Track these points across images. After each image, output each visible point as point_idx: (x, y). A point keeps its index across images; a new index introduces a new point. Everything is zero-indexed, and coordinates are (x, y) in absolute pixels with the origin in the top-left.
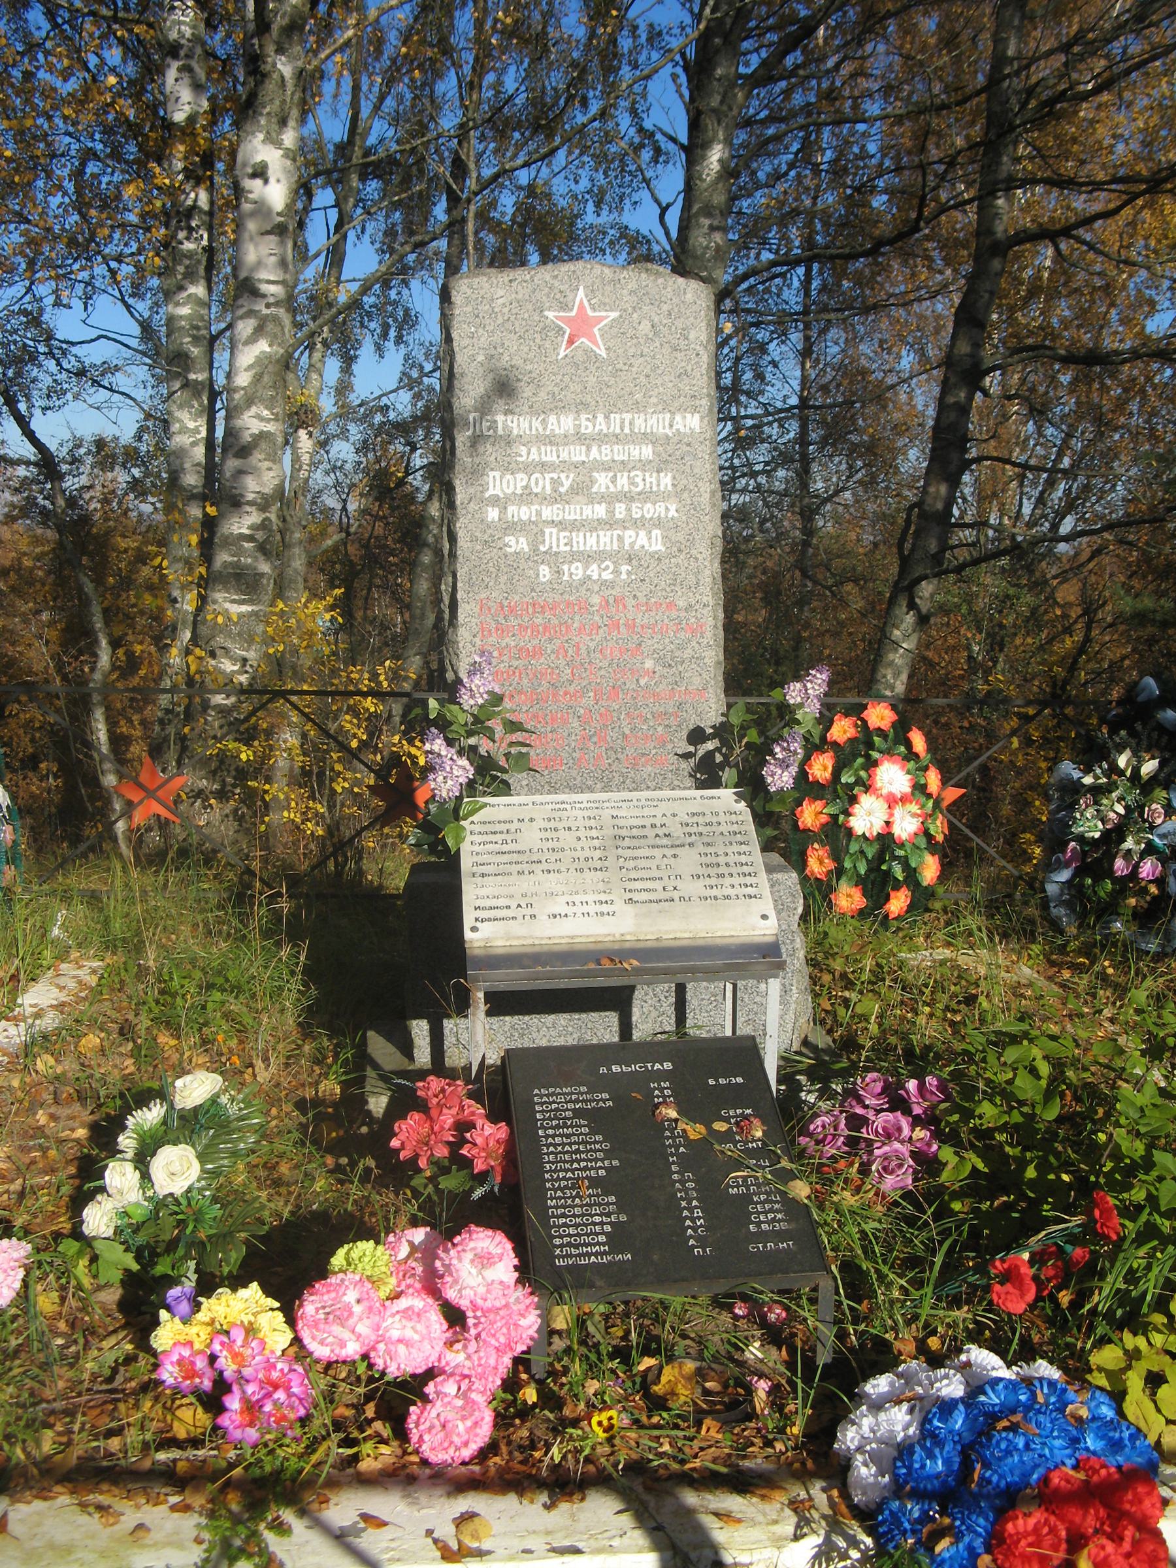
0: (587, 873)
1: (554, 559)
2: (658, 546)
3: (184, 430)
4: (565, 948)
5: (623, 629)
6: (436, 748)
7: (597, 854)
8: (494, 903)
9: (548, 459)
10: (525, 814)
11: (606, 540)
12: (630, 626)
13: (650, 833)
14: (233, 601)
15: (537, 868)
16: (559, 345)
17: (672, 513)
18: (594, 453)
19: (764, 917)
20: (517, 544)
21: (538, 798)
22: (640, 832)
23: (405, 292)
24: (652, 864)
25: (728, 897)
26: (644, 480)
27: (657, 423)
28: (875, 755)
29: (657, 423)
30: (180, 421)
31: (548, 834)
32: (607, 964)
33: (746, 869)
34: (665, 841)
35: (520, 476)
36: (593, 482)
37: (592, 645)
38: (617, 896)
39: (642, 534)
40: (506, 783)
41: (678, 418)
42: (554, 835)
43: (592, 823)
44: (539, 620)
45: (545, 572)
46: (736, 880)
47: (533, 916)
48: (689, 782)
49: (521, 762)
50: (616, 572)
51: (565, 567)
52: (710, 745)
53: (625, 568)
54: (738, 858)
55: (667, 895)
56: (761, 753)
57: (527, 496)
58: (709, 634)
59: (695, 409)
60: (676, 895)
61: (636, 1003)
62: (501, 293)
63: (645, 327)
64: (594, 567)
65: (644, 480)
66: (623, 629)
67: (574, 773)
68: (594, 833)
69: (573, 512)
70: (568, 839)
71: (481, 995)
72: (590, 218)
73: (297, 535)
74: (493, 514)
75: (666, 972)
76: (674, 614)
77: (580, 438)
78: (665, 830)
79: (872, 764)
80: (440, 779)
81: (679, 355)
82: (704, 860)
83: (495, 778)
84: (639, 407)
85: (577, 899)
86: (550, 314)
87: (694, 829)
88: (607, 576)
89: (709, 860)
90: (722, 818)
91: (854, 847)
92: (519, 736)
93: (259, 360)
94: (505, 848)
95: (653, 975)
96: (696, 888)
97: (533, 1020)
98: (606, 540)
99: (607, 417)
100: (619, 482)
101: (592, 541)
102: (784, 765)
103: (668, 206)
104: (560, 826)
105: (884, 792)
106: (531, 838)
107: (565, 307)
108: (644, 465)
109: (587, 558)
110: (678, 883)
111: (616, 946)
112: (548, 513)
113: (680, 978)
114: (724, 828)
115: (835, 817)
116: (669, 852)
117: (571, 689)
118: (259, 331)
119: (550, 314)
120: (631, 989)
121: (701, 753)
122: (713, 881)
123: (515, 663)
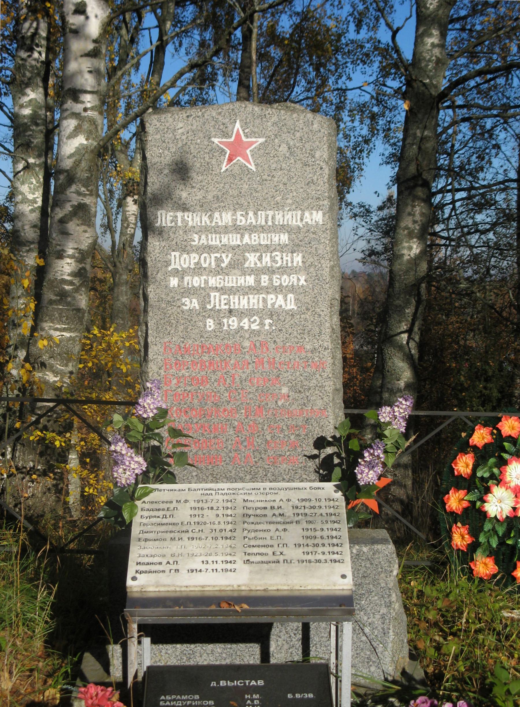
0: (221, 542)
1: (216, 314)
2: (291, 306)
3: (25, 200)
4: (199, 594)
5: (266, 365)
6: (118, 449)
7: (229, 527)
8: (150, 560)
9: (214, 243)
11: (254, 301)
12: (272, 363)
13: (269, 512)
14: (56, 329)
15: (185, 536)
16: (221, 163)
17: (302, 282)
18: (246, 239)
19: (344, 576)
20: (191, 304)
21: (193, 486)
22: (263, 512)
23: (211, 92)
25: (319, 561)
26: (282, 259)
27: (291, 218)
28: (506, 456)
29: (291, 218)
30: (22, 194)
31: (196, 512)
33: (335, 541)
34: (279, 519)
35: (193, 255)
36: (245, 260)
37: (244, 376)
38: (239, 558)
39: (280, 297)
40: (172, 474)
41: (307, 214)
42: (200, 512)
43: (229, 505)
44: (206, 358)
45: (210, 324)
46: (326, 549)
47: (177, 571)
48: (314, 476)
49: (182, 458)
50: (262, 324)
51: (225, 321)
52: (329, 450)
53: (268, 321)
54: (330, 533)
55: (275, 558)
56: (353, 459)
57: (198, 270)
58: (328, 370)
59: (319, 208)
60: (281, 558)
61: (273, 637)
62: (181, 125)
63: (284, 148)
64: (246, 320)
65: (282, 259)
66: (266, 365)
67: (230, 468)
68: (229, 512)
69: (231, 281)
70: (210, 515)
71: (135, 626)
72: (352, 35)
73: (124, 277)
74: (174, 282)
76: (303, 355)
77: (237, 229)
78: (280, 511)
79: (503, 463)
80: (121, 470)
81: (308, 169)
84: (278, 207)
85: (210, 559)
86: (216, 140)
87: (302, 511)
88: (254, 327)
89: (309, 533)
90: (323, 504)
91: (488, 526)
92: (183, 440)
93: (78, 149)
94: (165, 521)
97: (197, 648)
98: (254, 301)
99: (255, 214)
100: (264, 260)
101: (244, 302)
102: (371, 466)
103: (398, 29)
104: (205, 506)
105: (512, 485)
106: (184, 514)
107: (226, 135)
108: (282, 248)
109: (241, 314)
110: (285, 550)
111: (236, 594)
112: (213, 281)
113: (306, 620)
114: (323, 511)
115: (473, 503)
116: (281, 527)
117: (229, 408)
118: (77, 130)
119: (216, 140)
120: (269, 626)
121: (323, 456)
122: (310, 549)
123: (189, 388)
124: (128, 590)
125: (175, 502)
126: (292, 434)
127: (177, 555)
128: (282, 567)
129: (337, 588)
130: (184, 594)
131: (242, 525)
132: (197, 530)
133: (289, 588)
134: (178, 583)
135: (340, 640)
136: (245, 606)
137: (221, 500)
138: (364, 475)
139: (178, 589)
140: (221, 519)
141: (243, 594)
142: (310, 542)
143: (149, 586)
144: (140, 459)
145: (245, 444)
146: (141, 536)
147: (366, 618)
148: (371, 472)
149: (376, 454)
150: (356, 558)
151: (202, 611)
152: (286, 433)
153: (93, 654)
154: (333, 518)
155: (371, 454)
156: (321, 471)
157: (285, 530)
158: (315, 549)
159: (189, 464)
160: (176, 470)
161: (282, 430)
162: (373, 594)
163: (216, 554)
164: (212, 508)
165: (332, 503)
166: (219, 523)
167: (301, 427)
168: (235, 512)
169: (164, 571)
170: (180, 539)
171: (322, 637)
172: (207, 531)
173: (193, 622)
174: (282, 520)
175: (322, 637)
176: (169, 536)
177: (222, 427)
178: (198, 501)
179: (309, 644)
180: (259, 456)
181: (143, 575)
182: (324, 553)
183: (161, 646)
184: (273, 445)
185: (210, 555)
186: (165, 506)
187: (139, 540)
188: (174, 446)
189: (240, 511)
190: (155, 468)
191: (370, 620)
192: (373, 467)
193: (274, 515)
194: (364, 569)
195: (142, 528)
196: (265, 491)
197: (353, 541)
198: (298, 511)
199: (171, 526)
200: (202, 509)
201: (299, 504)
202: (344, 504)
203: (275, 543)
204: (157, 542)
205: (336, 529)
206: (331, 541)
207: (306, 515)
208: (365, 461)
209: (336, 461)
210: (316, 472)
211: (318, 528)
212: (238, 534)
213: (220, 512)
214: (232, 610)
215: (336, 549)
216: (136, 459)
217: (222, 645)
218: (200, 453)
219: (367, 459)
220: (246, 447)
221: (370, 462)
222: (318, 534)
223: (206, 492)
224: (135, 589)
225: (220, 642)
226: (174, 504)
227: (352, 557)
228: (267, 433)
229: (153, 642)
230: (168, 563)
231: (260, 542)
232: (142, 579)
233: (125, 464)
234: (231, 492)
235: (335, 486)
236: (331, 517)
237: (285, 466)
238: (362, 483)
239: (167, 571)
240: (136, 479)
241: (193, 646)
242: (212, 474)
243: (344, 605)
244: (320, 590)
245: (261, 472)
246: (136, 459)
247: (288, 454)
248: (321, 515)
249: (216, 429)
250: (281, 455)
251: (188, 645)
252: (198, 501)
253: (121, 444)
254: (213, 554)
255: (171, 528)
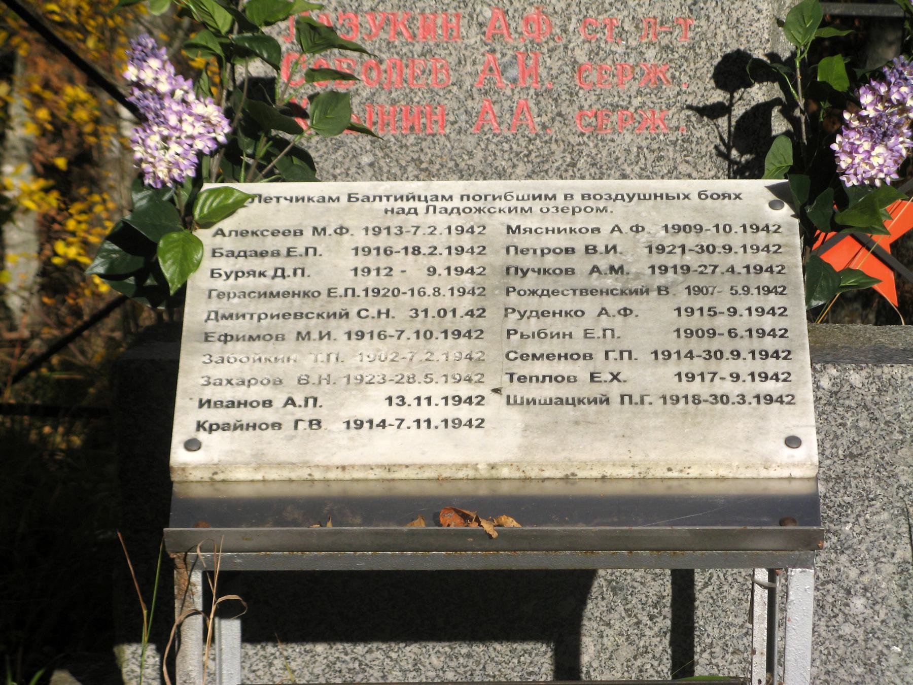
0: (440, 345)
4: (378, 490)
6: (147, 77)
7: (466, 303)
8: (240, 393)
10: (330, 219)
13: (581, 263)
15: (339, 328)
19: (793, 442)
21: (364, 187)
22: (564, 262)
24: (576, 327)
25: (723, 399)
31: (371, 261)
32: (452, 522)
33: (769, 344)
34: (610, 282)
42: (383, 261)
43: (466, 240)
46: (744, 366)
47: (315, 423)
49: (334, 110)
52: (759, 93)
54: (755, 321)
55: (596, 390)
56: (826, 113)
60: (615, 390)
61: (589, 626)
67: (469, 142)
68: (466, 261)
70: (411, 271)
71: (197, 577)
75: (660, 546)
78: (614, 260)
80: (154, 140)
82: (685, 322)
83: (281, 144)
85: (410, 392)
89: (696, 322)
90: (737, 239)
92: (333, 59)
94: (280, 285)
95: (627, 548)
96: (660, 378)
102: (879, 132)
104: (398, 243)
106: (335, 266)
110: (626, 369)
111: (483, 491)
113: (683, 561)
114: (738, 260)
116: (613, 304)
120: (586, 578)
121: (739, 111)
122: (697, 365)
124: (175, 477)
125: (308, 232)
126: (651, 44)
127: (314, 379)
128: (616, 414)
129: (772, 473)
130: (336, 490)
131: (502, 298)
132: (373, 312)
133: (635, 473)
134: (320, 459)
135: (778, 634)
136: (511, 523)
137: (442, 228)
138: (858, 158)
139: (317, 475)
140: (443, 281)
141: (505, 489)
142: (698, 345)
143: (234, 465)
144: (212, 111)
145: (513, 72)
146: (211, 326)
147: (853, 573)
148: (879, 149)
149: (895, 97)
150: (829, 404)
151: (386, 533)
152: (633, 43)
153: (75, 674)
154: (766, 279)
155: (881, 99)
156: (734, 153)
157: (626, 312)
158: (713, 365)
159: (353, 128)
160: (311, 141)
161: (622, 33)
162: (878, 504)
163: (428, 379)
164: (417, 251)
165: (762, 238)
166: (437, 291)
167: (676, 23)
168: (483, 260)
169: (277, 426)
170: (325, 335)
171: (729, 625)
172: (401, 314)
173: (361, 565)
174: (619, 284)
175: (729, 625)
176: (292, 326)
177: (447, 22)
178: (377, 231)
179: (692, 646)
180: (552, 109)
181: (217, 435)
182: (736, 377)
183: (270, 649)
184: (594, 77)
185: (411, 380)
186: (281, 243)
187: (207, 337)
188: (313, 75)
189: (496, 259)
190: (257, 139)
191: (865, 579)
192: (885, 135)
193: (595, 269)
194: (853, 434)
195: (214, 305)
196: (570, 204)
197: (821, 355)
198: (662, 259)
199: (297, 301)
200: (388, 252)
201: (668, 241)
202: (798, 241)
203: (597, 348)
204: (258, 344)
205: (772, 311)
206: (757, 344)
207: (687, 269)
208: (862, 119)
209: (779, 125)
210: (720, 154)
211: (722, 307)
212: (492, 321)
213: (440, 262)
214: (473, 534)
215: (771, 366)
216: (199, 109)
217: (444, 648)
218: (382, 98)
219: (870, 112)
220: (514, 81)
221: (876, 122)
222: (722, 323)
223: (400, 204)
224: (195, 475)
225: (439, 639)
226: (308, 239)
227: (817, 400)
228: (576, 41)
229: (249, 636)
230: (291, 401)
231: (555, 346)
232: (216, 447)
233: (165, 122)
234: (471, 204)
235: (772, 188)
236: (761, 276)
237: (628, 137)
238: (851, 182)
239: (288, 424)
240: (199, 168)
241: (360, 649)
242: (418, 162)
243: (794, 522)
244: (724, 479)
245: (558, 156)
246: (199, 109)
247: (636, 102)
248: (732, 270)
249: (428, 29)
250: (615, 107)
251: (348, 646)
252: (377, 231)
253: (154, 63)
254: (420, 377)
255: (297, 304)
